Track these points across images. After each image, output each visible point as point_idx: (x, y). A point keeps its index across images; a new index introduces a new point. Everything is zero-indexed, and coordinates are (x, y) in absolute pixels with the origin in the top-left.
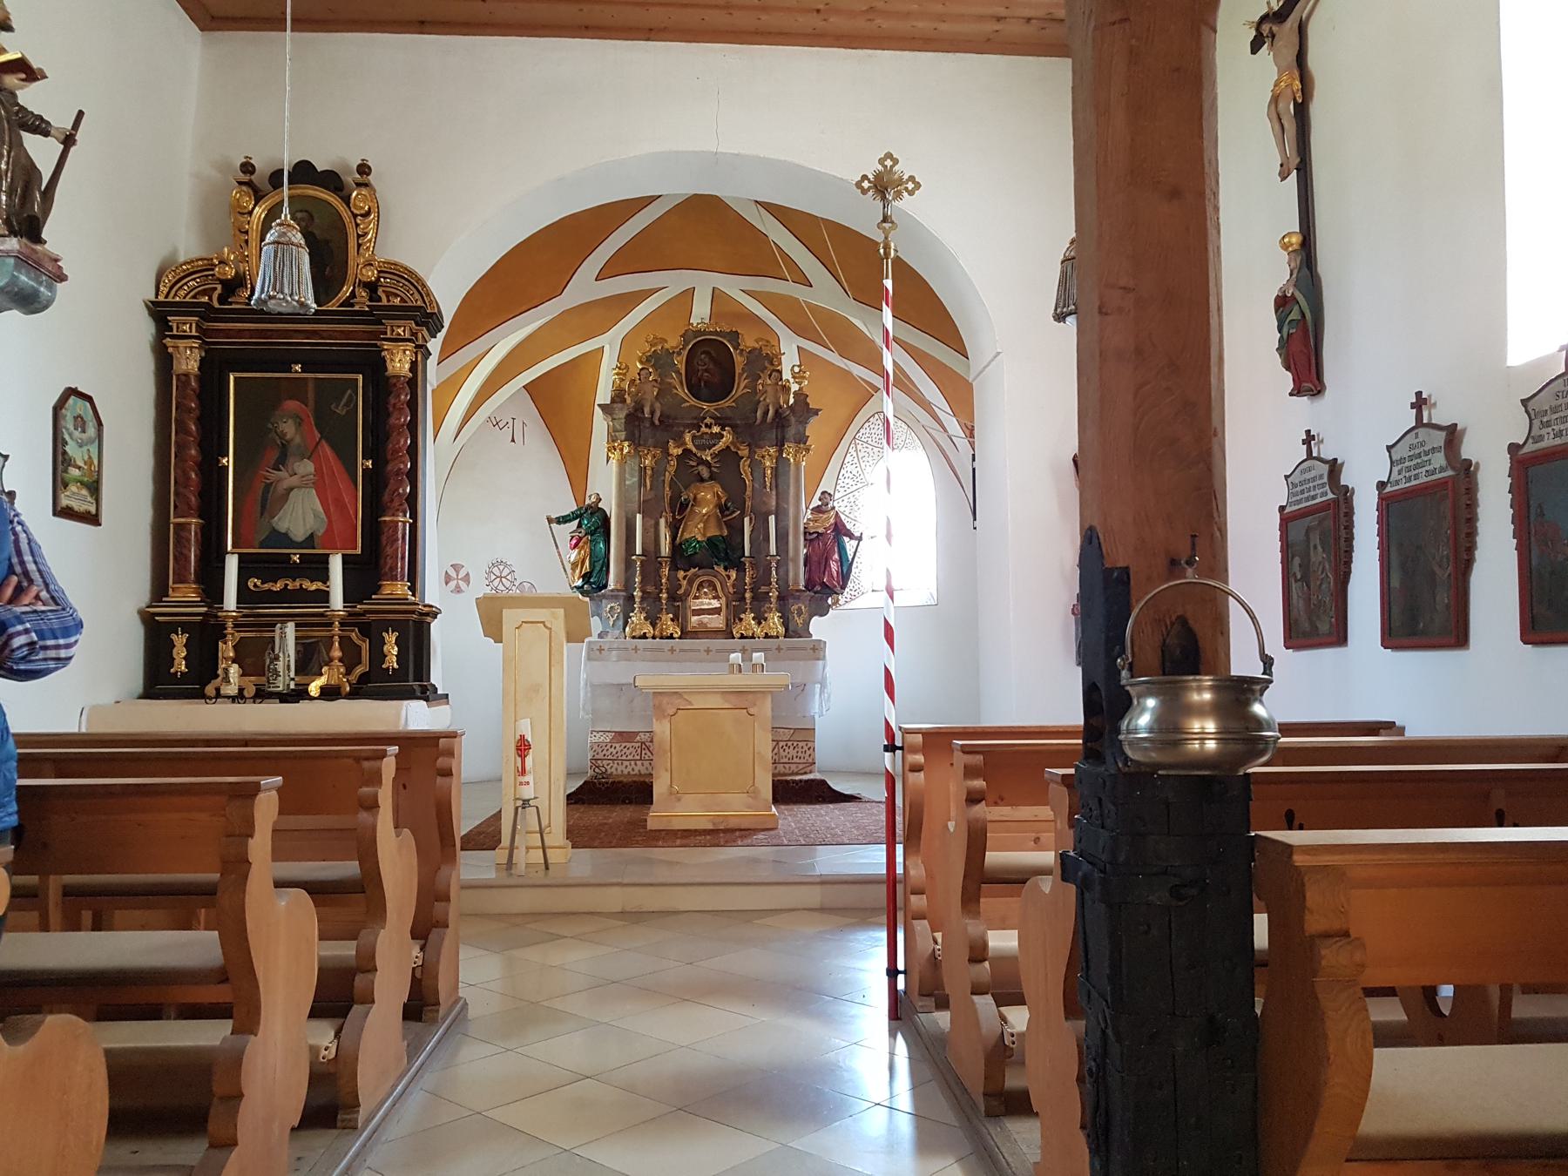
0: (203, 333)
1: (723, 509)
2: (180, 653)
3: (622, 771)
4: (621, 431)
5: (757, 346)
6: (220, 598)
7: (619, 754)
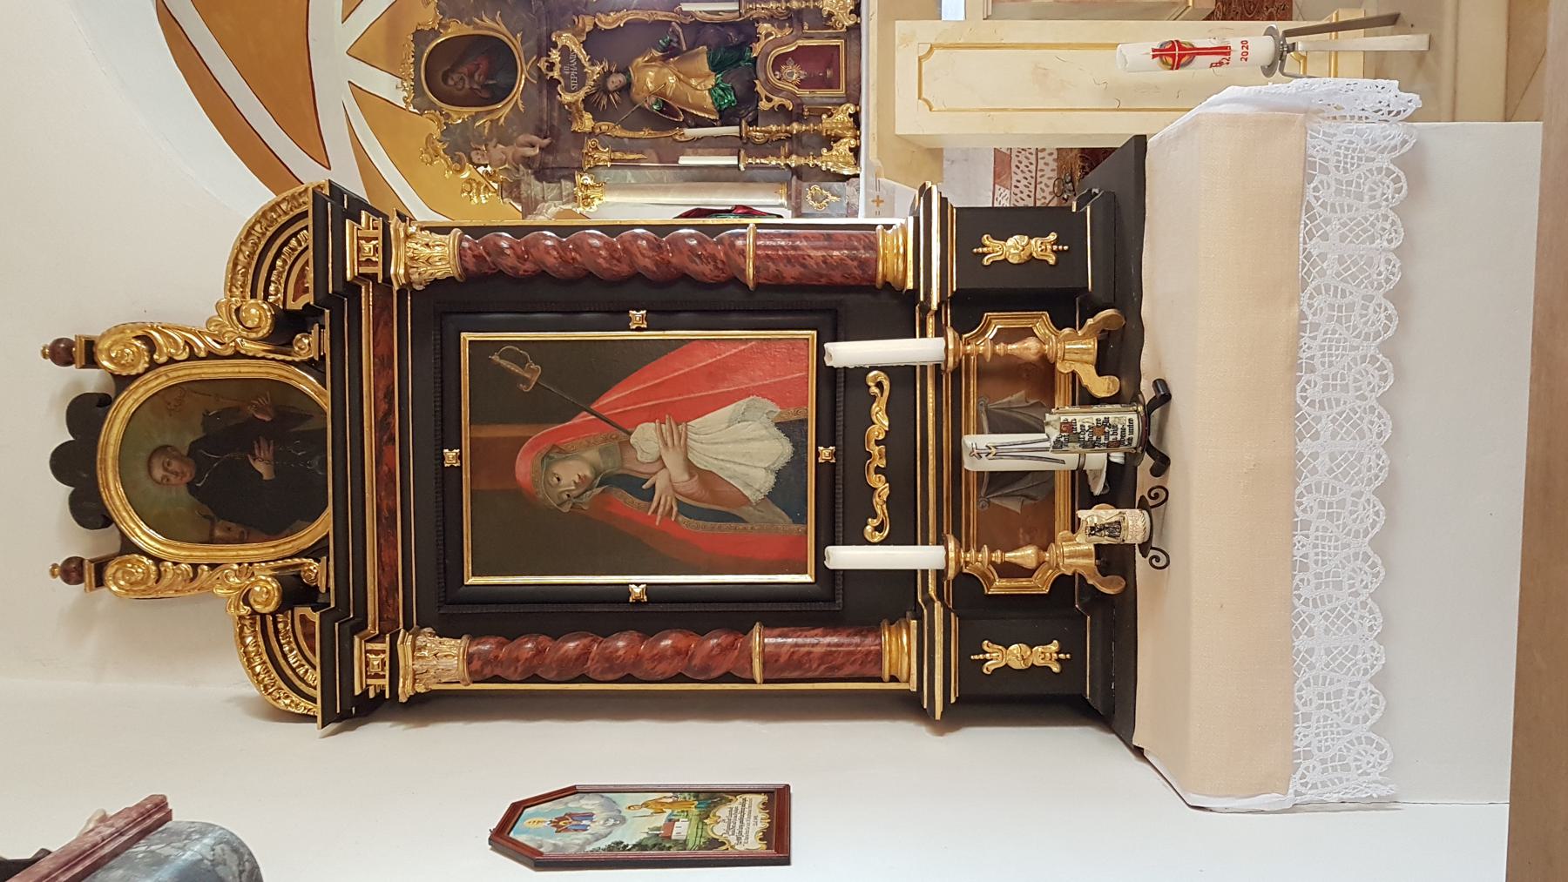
0: (389, 630)
1: (670, 52)
2: (1016, 655)
3: (1053, 170)
4: (560, 188)
6: (907, 578)
7: (1028, 175)
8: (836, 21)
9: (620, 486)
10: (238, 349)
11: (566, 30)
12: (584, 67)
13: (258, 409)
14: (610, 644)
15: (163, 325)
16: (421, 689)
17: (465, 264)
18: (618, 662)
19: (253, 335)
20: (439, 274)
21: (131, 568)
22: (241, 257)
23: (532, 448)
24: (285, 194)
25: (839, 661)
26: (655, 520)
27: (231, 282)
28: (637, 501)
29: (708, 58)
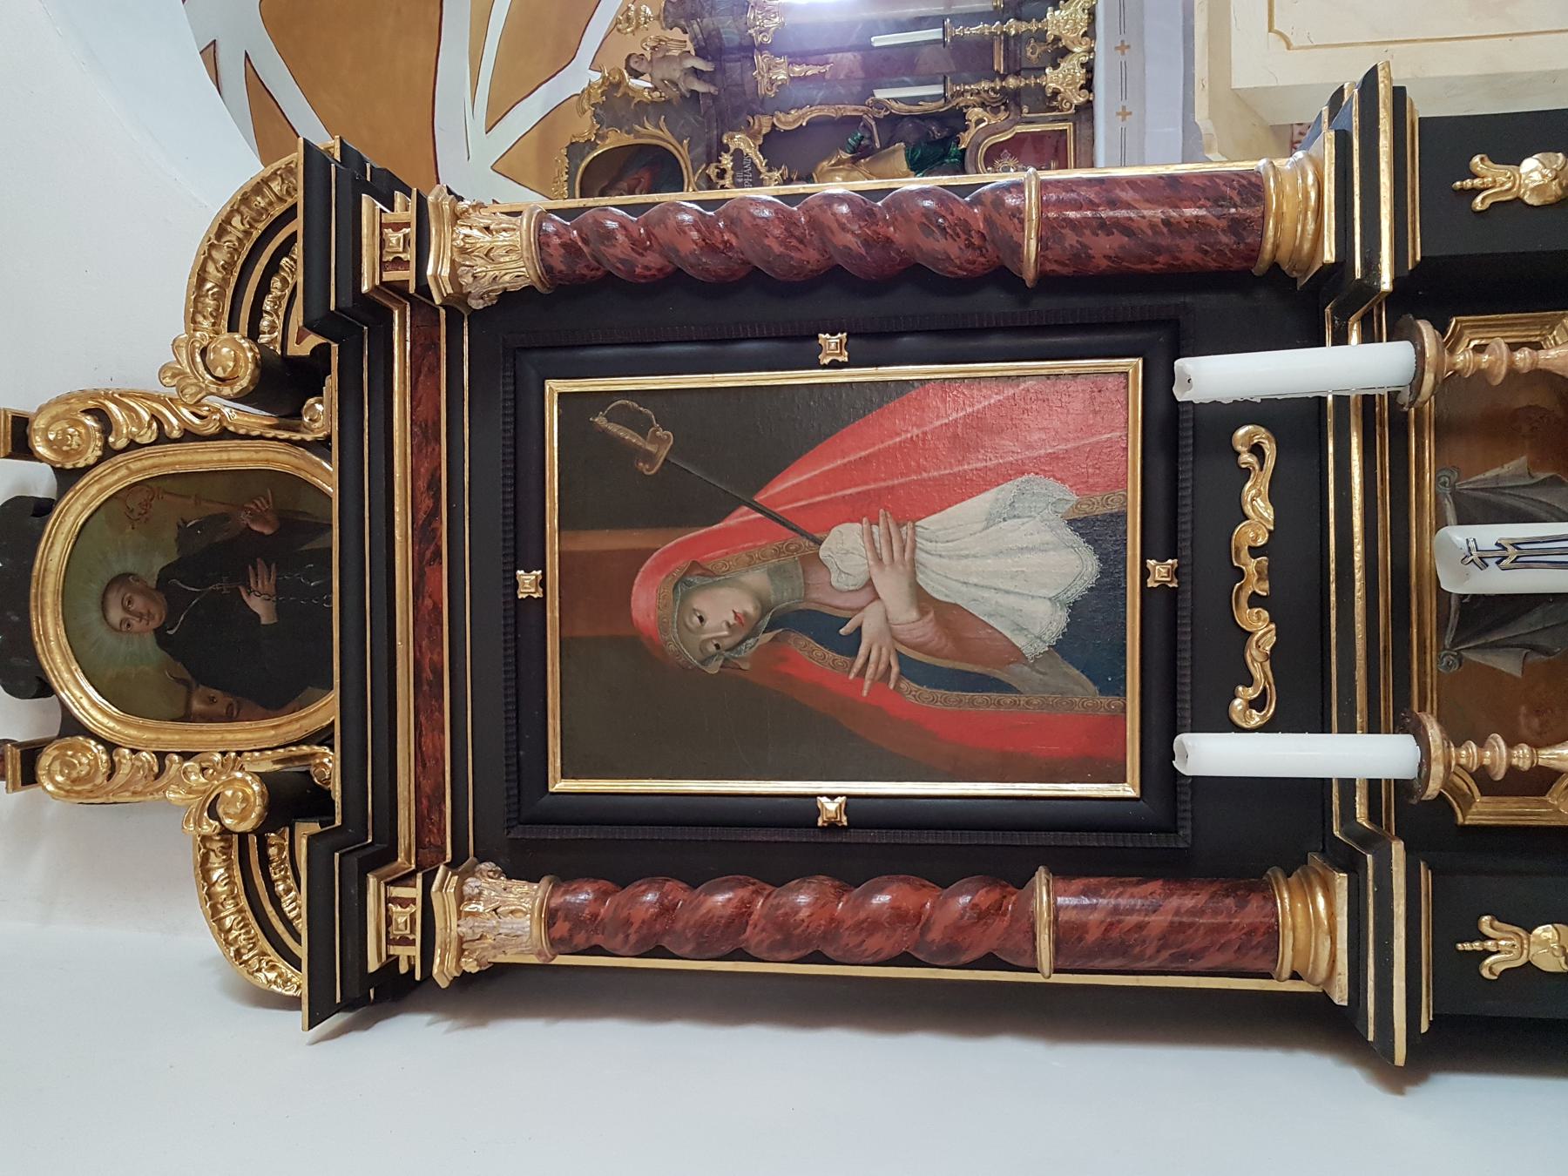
5: (589, 113)
8: (1062, 100)
9: (801, 631)
10: (225, 424)
11: (740, 131)
12: (760, 173)
13: (256, 517)
14: (784, 899)
15: (122, 391)
16: (471, 967)
17: (548, 258)
18: (799, 931)
19: (226, 390)
20: (507, 278)
21: (71, 756)
22: (211, 268)
23: (659, 568)
24: (276, 165)
25: (1197, 943)
26: (862, 689)
27: (195, 307)
28: (831, 655)
29: (907, 155)
